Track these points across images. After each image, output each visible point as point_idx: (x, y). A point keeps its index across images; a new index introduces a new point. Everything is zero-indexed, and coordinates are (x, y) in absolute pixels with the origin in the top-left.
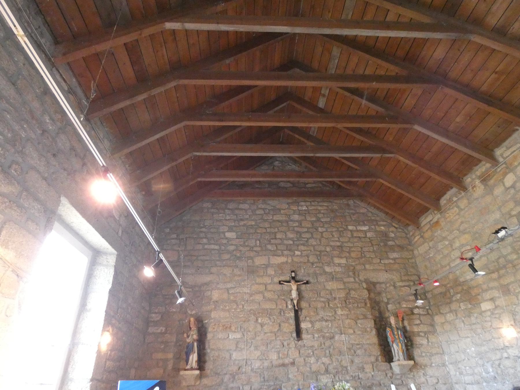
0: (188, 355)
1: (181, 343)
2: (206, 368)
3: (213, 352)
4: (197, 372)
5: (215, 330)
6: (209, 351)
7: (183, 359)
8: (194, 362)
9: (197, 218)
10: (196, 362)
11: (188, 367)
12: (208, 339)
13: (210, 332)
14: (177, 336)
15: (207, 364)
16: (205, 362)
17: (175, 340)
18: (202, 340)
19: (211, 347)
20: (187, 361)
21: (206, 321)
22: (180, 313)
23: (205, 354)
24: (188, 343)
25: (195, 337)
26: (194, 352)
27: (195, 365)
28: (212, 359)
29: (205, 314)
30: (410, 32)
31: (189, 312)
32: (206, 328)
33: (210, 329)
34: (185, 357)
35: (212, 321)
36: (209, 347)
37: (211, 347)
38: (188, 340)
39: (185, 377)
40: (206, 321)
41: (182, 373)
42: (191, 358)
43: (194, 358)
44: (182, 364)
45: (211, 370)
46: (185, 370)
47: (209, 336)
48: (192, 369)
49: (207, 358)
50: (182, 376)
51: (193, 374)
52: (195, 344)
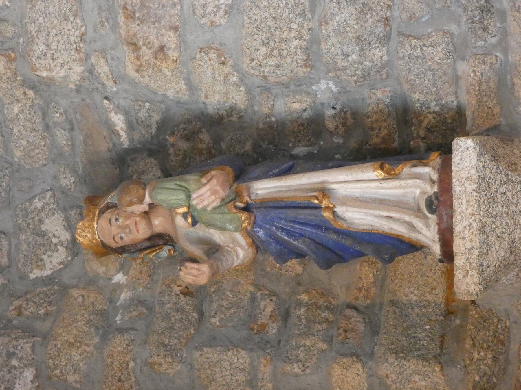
0: (340, 247)
1: (268, 307)
2: (450, 100)
3: (331, 47)
4: (466, 152)
5: (171, 40)
6: (325, 89)
7: (381, 283)
8: (392, 189)
9: (355, 360)
10: (391, 176)
11: (427, 234)
12: (238, 98)
13: (191, 87)
14: (212, 342)
15: (417, 97)
16: (404, 114)
17: (242, 358)
18: (239, 146)
19: (292, 64)
20: (393, 248)
21: (118, 121)
22: (46, 337)
23: (352, 119)
24: (256, 245)
25: (208, 192)
26: (324, 192)
27: (414, 183)
28: (378, 53)
29: (62, 137)
30: (271, 181)
31: (54, 260)
32: (165, 125)
33: (171, 88)
34: (364, 271)
35: (103, 69)
36: (297, 85)
37: (292, 64)
38: (240, 251)
39: (498, 253)
40: (118, 121)
41: (467, 283)
42: (359, 218)
43: (363, 196)
44: (412, 285)
45: (458, 50)
46: (448, 255)
47: (218, 91)
48: (440, 203)
49: (378, 97)
50: (488, 284)
51: (483, 183)
52: (264, 188)
